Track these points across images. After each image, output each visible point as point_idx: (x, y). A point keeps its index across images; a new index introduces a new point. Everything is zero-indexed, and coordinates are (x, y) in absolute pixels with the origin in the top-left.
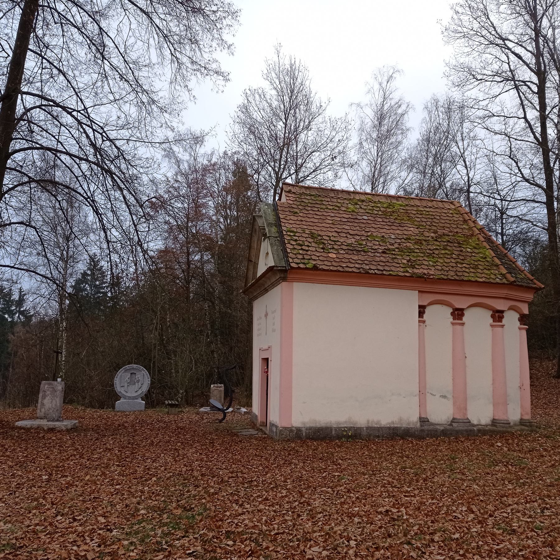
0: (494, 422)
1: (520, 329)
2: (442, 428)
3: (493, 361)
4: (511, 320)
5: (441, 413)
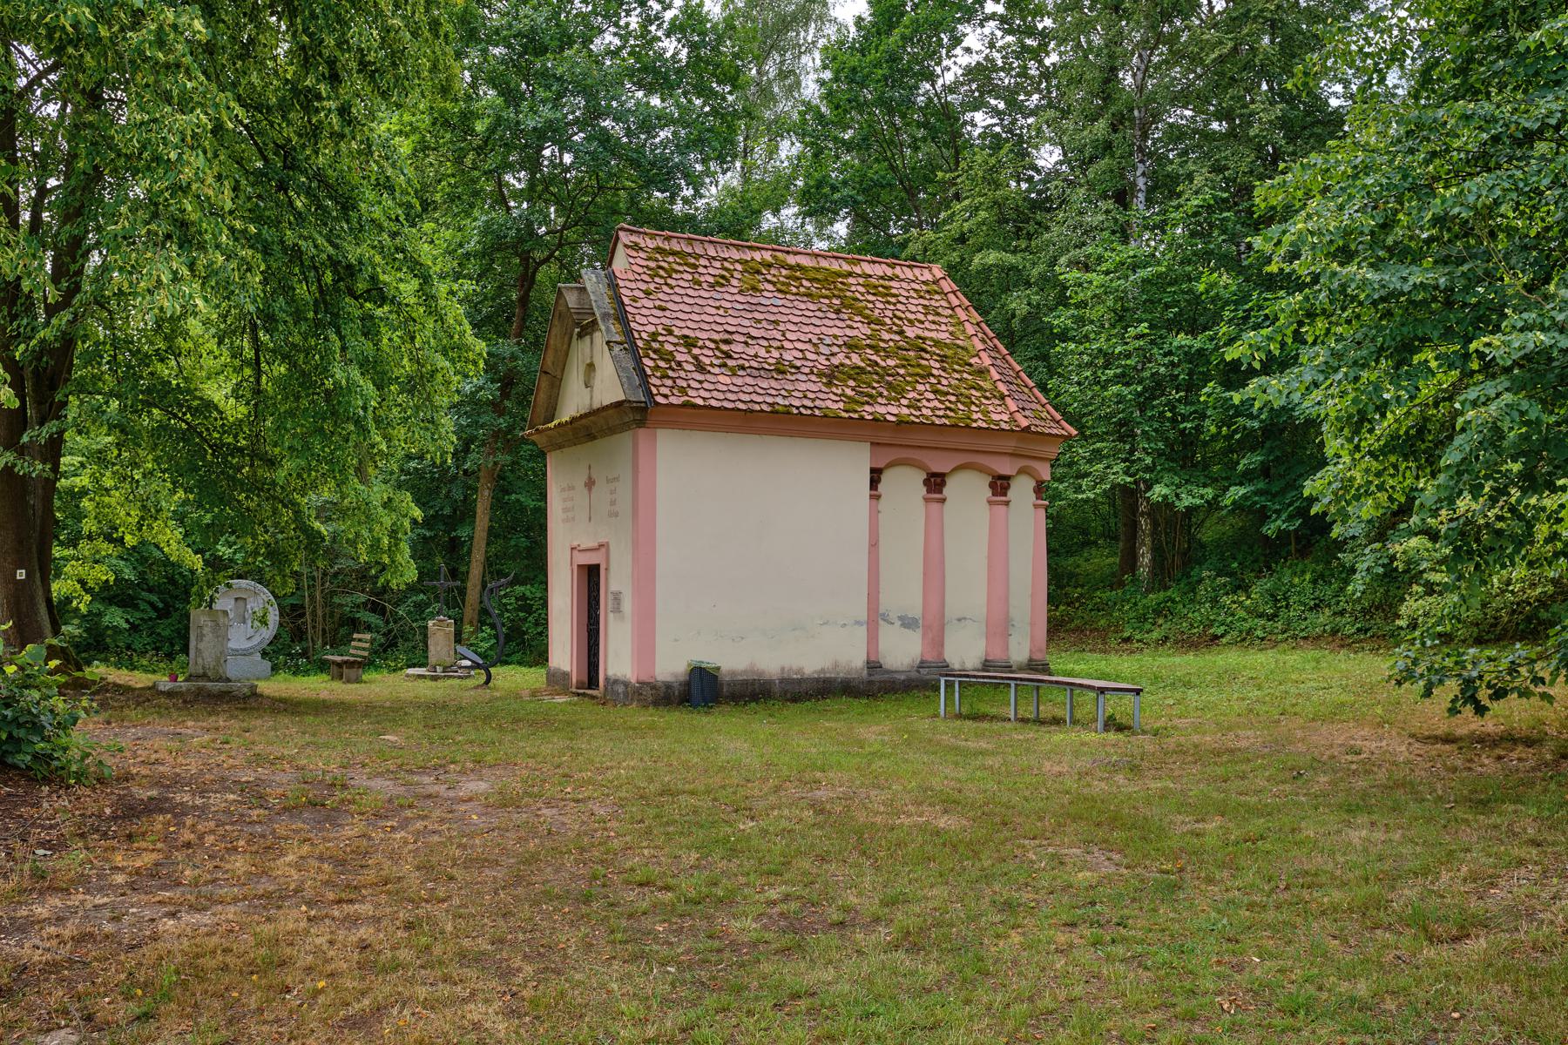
0: (987, 665)
1: (1036, 506)
2: (903, 677)
3: (990, 558)
4: (1022, 490)
5: (902, 651)
